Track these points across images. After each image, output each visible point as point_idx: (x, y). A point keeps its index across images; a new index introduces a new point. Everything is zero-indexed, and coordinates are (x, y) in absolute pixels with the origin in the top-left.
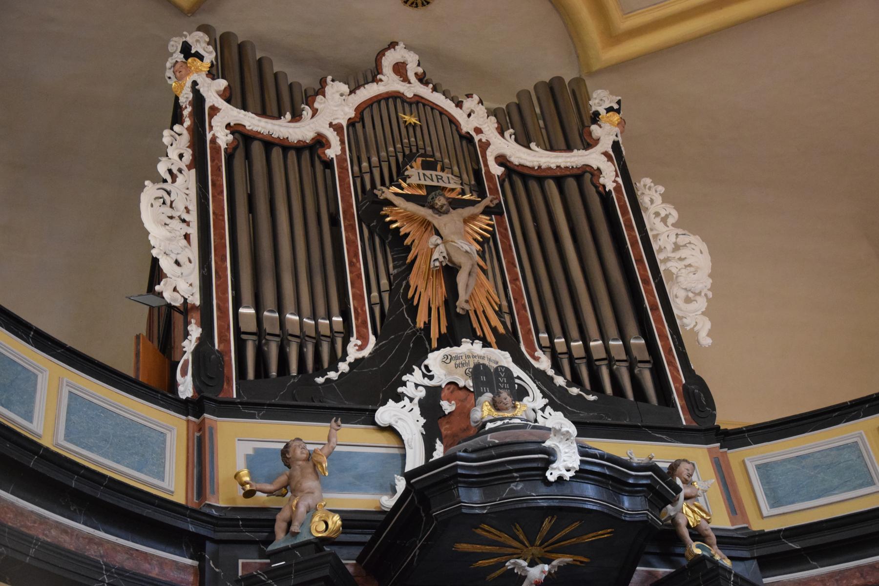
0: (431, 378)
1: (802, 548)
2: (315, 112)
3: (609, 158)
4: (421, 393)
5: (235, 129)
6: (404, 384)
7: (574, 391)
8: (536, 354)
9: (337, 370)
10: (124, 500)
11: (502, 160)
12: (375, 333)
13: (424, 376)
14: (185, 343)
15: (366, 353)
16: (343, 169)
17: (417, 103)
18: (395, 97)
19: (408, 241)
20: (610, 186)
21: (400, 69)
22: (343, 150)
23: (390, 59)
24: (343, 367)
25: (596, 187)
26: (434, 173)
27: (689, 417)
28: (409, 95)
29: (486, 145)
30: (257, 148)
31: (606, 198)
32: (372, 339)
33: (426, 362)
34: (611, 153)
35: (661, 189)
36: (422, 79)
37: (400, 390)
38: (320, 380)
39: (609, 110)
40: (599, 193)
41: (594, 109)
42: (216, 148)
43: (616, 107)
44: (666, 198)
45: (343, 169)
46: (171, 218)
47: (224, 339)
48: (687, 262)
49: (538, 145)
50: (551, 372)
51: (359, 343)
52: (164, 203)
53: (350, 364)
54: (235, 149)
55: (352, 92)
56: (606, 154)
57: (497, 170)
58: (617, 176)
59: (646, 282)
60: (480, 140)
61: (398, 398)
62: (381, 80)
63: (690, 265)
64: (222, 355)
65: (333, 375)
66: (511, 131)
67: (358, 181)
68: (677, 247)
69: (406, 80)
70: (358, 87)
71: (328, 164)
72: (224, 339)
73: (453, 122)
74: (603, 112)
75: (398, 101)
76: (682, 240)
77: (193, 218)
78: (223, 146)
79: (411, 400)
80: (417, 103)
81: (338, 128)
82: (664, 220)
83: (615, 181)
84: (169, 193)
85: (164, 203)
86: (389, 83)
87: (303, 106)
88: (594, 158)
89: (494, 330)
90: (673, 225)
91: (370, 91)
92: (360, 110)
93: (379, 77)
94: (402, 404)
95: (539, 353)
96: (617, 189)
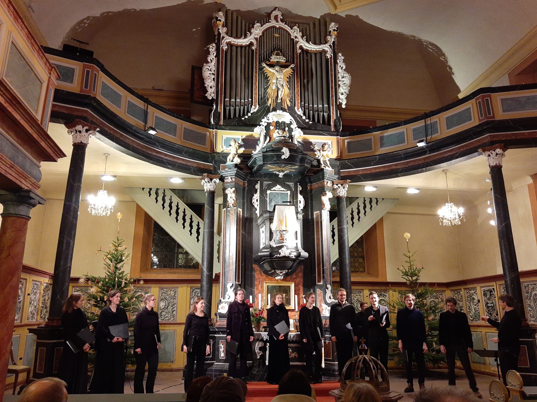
0: (269, 120)
1: (59, 118)
2: (251, 33)
3: (331, 47)
4: (266, 124)
5: (229, 44)
6: (262, 122)
7: (307, 120)
8: (299, 110)
9: (248, 116)
10: (311, 129)
11: (301, 48)
12: (259, 104)
13: (267, 119)
14: (256, 212)
15: (255, 110)
16: (256, 53)
17: (280, 29)
18: (273, 27)
19: (269, 79)
20: (329, 56)
21: (276, 18)
22: (257, 47)
23: (273, 16)
24: (249, 114)
25: (326, 57)
26: (279, 56)
27: (334, 128)
28: (278, 26)
29: (297, 42)
30: (234, 49)
31: (327, 60)
32: (258, 106)
33: (268, 116)
34: (332, 45)
35: (343, 58)
36: (282, 21)
37: (261, 123)
38: (243, 119)
39: (334, 30)
40: (326, 59)
41: (330, 30)
42: (223, 50)
43: (336, 29)
44: (344, 61)
45: (256, 53)
46: (210, 74)
47: (221, 109)
48: (344, 82)
49: (312, 43)
50: (302, 115)
51: (254, 107)
52: (208, 70)
53: (252, 114)
54: (228, 50)
55: (262, 26)
56: (330, 46)
57: (299, 51)
58: (332, 53)
59: (332, 88)
60: (296, 41)
61: (260, 125)
62: (270, 22)
63: (345, 83)
64: (220, 113)
65: (246, 117)
66: (305, 37)
67: (260, 57)
68: (343, 77)
69: (277, 22)
70: (264, 24)
71: (253, 51)
72: (221, 109)
73: (289, 35)
74: (332, 31)
75: (275, 28)
76: (345, 75)
77: (215, 73)
78: (225, 50)
79: (263, 126)
80: (280, 29)
81: (256, 39)
82: (342, 68)
83: (331, 55)
84: (210, 66)
85: (208, 70)
86: (273, 23)
87: (248, 32)
88: (326, 47)
89: (288, 105)
90: (344, 70)
91: (267, 25)
92: (263, 33)
93: (270, 20)
94: (261, 127)
95: (300, 109)
96: (331, 58)
